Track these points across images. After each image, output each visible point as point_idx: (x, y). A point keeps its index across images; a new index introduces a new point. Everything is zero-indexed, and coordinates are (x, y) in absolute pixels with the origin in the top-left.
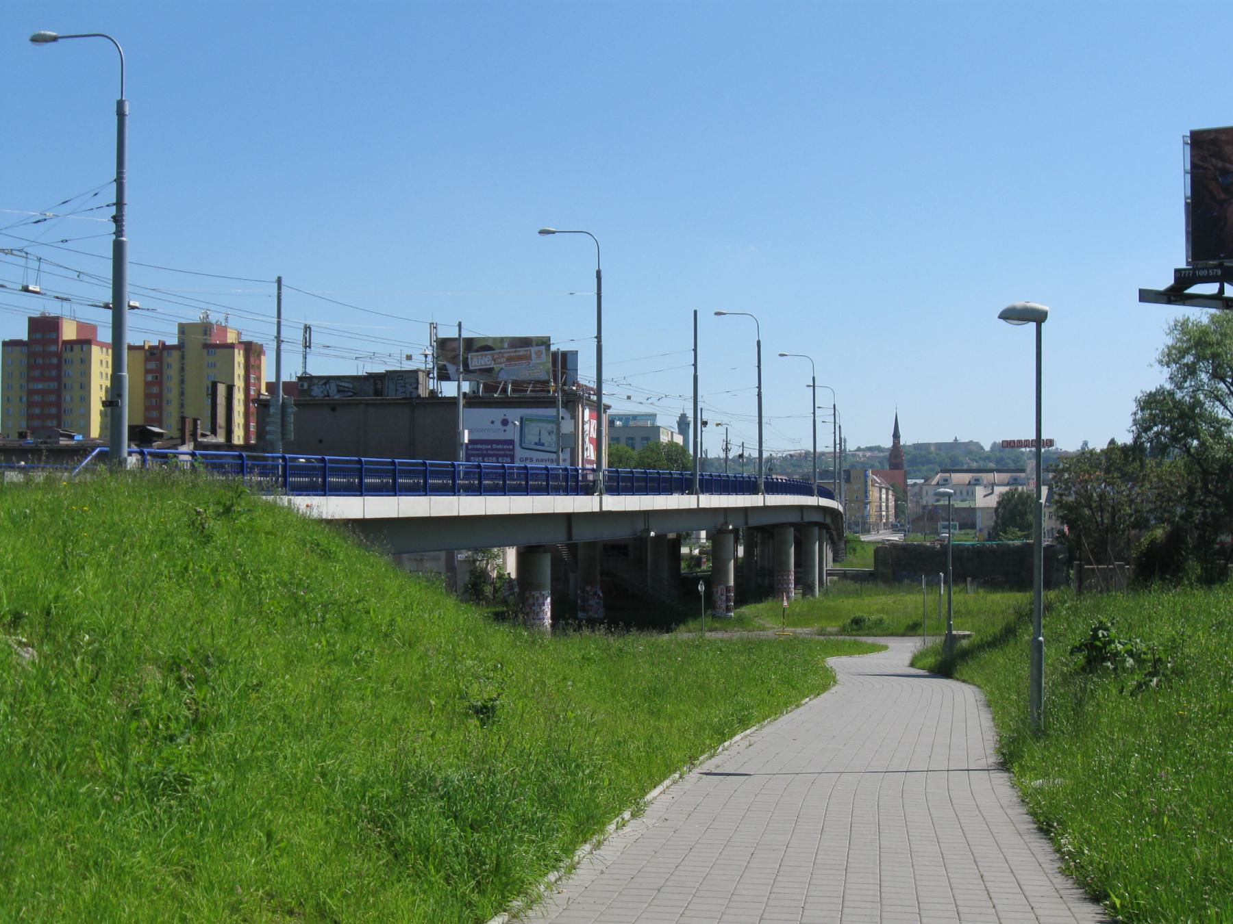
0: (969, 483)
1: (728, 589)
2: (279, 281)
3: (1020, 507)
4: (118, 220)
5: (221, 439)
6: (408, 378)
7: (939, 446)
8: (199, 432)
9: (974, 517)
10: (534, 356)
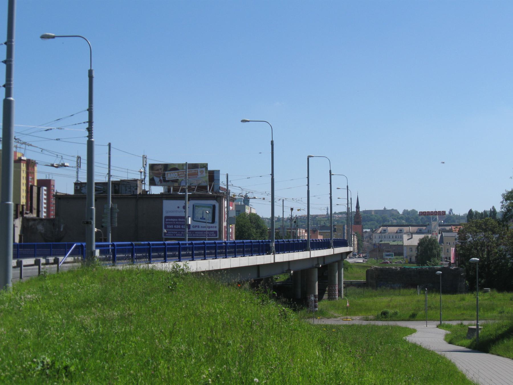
0: (397, 232)
1: (315, 296)
2: (110, 145)
3: (430, 246)
4: (90, 130)
5: (34, 215)
6: (132, 184)
7: (377, 212)
8: (25, 211)
9: (403, 250)
10: (199, 173)
